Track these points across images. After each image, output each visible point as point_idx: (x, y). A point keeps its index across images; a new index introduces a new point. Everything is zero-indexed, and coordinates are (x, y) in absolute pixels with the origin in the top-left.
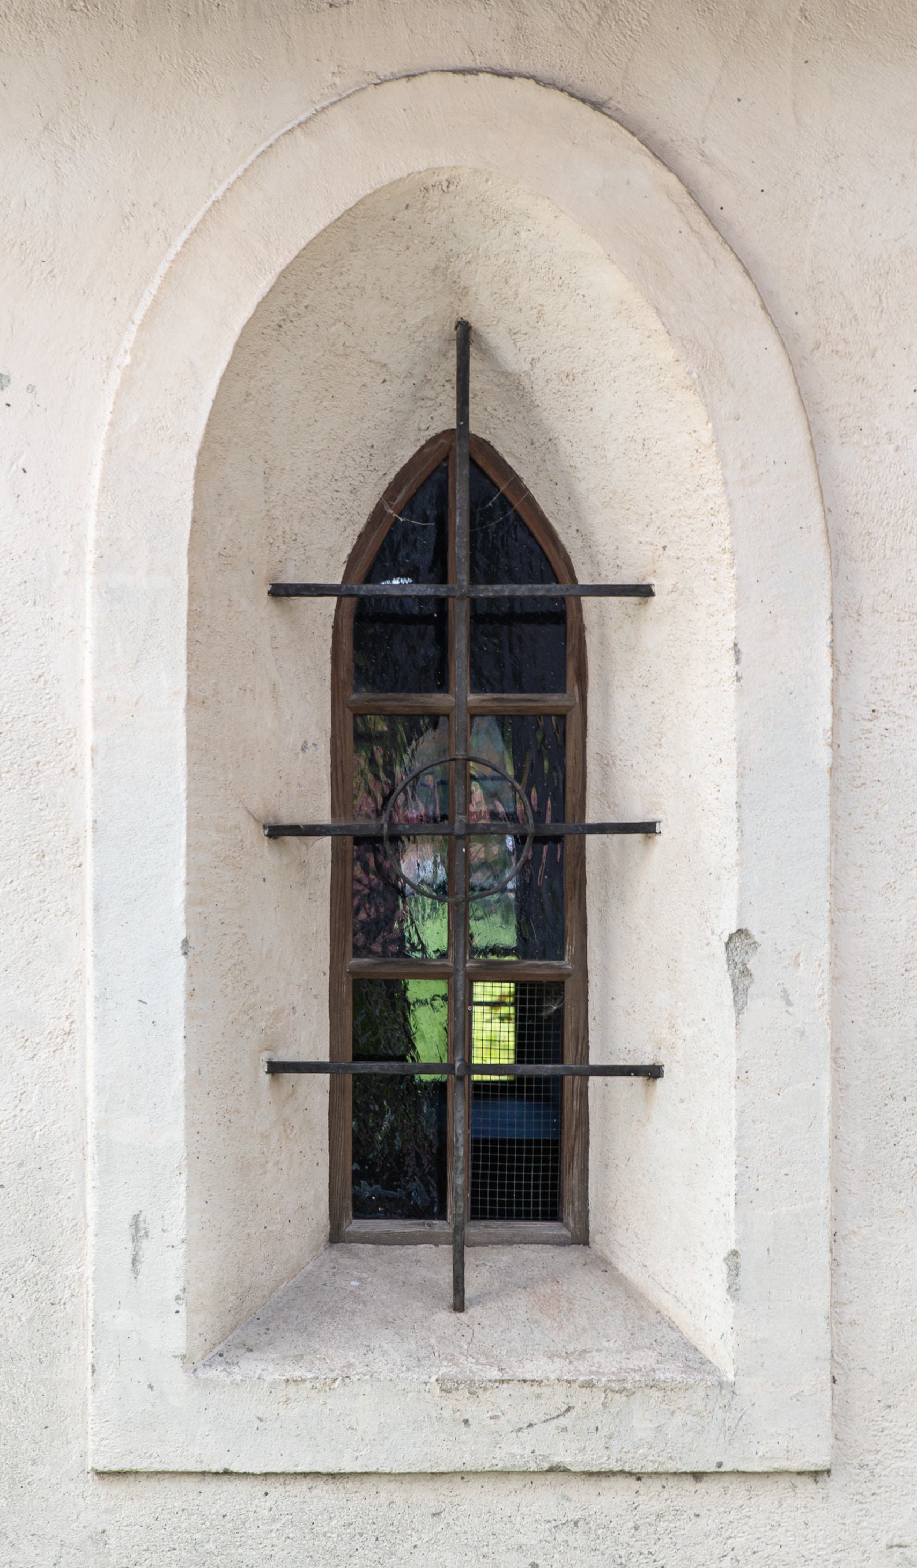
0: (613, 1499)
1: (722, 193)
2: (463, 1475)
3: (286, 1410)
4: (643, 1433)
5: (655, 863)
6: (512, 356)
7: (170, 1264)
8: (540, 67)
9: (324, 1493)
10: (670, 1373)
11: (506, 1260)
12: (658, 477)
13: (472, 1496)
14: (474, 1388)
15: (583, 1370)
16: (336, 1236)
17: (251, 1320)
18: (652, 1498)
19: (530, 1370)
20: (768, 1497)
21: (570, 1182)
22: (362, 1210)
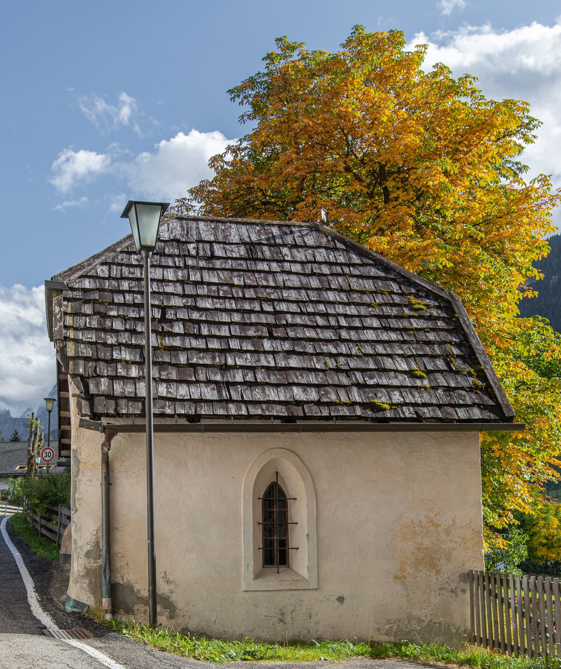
0: (296, 593)
1: (304, 461)
2: (281, 590)
3: (262, 584)
4: (300, 585)
5: (297, 527)
6: (282, 475)
7: (251, 569)
8: (286, 447)
9: (267, 593)
10: (301, 579)
11: (282, 568)
12: (296, 485)
13: (282, 593)
14: (282, 581)
15: (293, 579)
16: (263, 567)
17: (257, 576)
18: (300, 592)
19: (288, 579)
20: (311, 592)
21: (287, 561)
22: (266, 564)
